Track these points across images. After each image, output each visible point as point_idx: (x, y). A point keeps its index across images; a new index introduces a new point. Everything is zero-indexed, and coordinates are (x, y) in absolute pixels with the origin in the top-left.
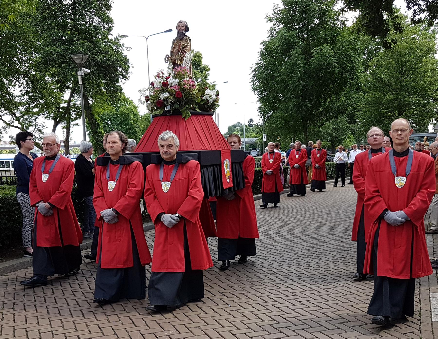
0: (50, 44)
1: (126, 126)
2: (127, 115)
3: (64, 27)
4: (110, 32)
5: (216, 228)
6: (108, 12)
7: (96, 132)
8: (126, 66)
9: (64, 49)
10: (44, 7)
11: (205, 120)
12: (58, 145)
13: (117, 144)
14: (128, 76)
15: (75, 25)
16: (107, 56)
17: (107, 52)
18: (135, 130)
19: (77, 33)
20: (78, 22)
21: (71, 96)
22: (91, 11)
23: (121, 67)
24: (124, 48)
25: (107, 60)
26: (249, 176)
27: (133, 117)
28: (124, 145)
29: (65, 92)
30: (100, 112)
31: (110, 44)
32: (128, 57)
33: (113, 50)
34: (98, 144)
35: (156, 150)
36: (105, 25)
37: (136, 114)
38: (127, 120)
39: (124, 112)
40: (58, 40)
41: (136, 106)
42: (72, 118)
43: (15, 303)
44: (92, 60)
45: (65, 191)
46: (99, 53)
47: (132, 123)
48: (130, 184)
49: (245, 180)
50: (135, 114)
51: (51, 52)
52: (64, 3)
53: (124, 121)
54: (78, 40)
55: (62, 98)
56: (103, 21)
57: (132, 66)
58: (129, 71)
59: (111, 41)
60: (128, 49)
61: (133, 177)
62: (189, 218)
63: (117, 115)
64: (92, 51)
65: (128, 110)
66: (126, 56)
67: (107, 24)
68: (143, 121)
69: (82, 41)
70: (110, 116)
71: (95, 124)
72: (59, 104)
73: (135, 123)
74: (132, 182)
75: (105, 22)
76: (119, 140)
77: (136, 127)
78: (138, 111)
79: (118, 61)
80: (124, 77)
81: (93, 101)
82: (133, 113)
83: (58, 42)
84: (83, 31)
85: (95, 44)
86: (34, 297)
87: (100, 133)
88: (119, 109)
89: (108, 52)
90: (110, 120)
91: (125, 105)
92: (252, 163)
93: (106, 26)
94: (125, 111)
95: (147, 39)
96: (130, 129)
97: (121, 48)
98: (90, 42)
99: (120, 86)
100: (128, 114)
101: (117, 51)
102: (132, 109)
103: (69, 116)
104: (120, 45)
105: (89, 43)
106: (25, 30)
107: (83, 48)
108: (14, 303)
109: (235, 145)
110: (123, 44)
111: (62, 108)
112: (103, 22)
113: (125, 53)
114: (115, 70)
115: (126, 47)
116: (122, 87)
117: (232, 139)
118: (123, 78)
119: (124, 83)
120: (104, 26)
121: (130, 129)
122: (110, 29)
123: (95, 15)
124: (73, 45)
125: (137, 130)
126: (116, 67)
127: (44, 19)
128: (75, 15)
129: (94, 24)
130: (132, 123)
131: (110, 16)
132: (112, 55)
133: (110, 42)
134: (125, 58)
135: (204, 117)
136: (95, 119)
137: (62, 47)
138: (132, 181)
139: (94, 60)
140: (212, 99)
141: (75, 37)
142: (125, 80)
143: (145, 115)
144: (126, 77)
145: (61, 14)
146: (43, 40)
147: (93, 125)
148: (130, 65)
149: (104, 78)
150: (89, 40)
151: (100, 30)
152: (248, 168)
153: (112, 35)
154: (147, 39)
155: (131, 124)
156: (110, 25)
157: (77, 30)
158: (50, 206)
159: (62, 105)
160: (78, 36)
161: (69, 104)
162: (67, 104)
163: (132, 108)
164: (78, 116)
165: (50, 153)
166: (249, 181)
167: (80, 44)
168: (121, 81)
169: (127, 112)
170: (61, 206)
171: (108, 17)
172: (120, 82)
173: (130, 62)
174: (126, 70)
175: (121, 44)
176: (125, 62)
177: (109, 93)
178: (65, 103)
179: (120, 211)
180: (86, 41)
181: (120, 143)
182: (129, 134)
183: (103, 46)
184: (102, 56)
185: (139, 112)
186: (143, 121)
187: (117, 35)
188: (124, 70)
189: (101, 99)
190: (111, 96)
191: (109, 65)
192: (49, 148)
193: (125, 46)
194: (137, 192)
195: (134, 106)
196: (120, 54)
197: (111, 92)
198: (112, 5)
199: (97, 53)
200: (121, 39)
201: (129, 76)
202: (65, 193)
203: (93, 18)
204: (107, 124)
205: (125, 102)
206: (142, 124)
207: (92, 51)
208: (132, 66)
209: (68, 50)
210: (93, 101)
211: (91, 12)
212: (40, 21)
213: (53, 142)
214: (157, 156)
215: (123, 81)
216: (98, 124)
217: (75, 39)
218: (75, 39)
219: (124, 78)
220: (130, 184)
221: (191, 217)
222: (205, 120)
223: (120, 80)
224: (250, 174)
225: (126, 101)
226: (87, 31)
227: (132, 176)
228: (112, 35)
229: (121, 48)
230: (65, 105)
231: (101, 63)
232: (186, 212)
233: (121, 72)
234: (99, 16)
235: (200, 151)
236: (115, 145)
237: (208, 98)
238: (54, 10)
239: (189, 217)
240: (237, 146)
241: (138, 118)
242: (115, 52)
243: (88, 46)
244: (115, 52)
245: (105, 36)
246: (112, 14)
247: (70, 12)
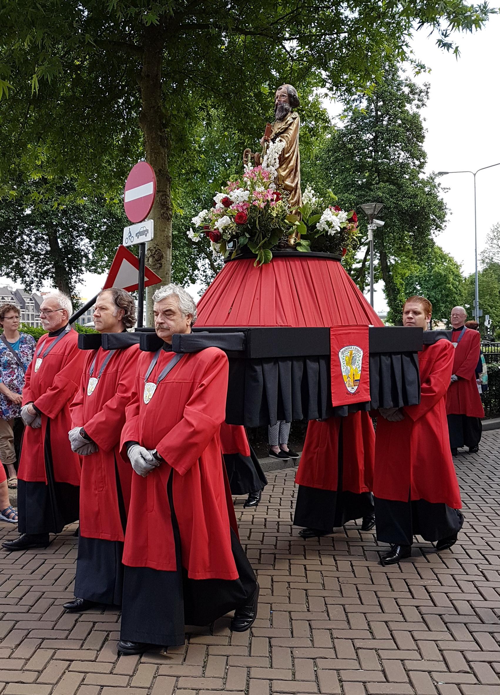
0: (342, 191)
1: (441, 291)
2: (445, 276)
3: (361, 168)
4: (422, 170)
5: (373, 468)
6: (420, 144)
7: (395, 299)
8: (441, 212)
9: (359, 196)
10: (337, 146)
11: (307, 270)
12: (65, 312)
13: (106, 312)
14: (443, 226)
15: (375, 164)
16: (416, 201)
17: (415, 196)
18: (455, 297)
19: (376, 174)
20: (379, 161)
21: (367, 253)
22: (398, 144)
23: (434, 213)
24: (439, 189)
25: (415, 206)
26: (434, 378)
27: (453, 279)
28: (123, 312)
29: (360, 249)
30: (405, 274)
31: (421, 185)
32: (444, 201)
33: (424, 192)
34: (396, 316)
35: (237, 324)
36: (415, 161)
37: (457, 276)
38: (443, 283)
39: (440, 274)
40: (353, 184)
41: (459, 264)
42: (367, 281)
43: (244, 513)
44: (394, 208)
45: (58, 388)
46: (405, 197)
47: (450, 287)
48: (118, 384)
49: (425, 385)
50: (456, 276)
51: (343, 200)
52: (364, 138)
53: (439, 285)
54: (377, 184)
55: (355, 257)
56: (412, 156)
57: (450, 211)
58: (445, 219)
59: (423, 181)
60: (446, 190)
61: (125, 372)
62: (173, 463)
63: (430, 276)
64: (395, 195)
65: (445, 270)
66: (442, 199)
67: (418, 159)
68: (467, 285)
69: (382, 184)
70: (420, 278)
71: (394, 290)
72: (350, 265)
73: (455, 288)
74: (121, 382)
75: (415, 157)
76: (112, 303)
77: (457, 294)
78: (461, 271)
79: (430, 207)
80: (438, 227)
81: (395, 260)
82: (453, 274)
83: (352, 187)
84: (385, 171)
85: (400, 186)
86: (268, 509)
87: (401, 302)
88: (433, 268)
89: (417, 195)
90: (420, 284)
91: (443, 264)
92: (446, 354)
93: (417, 163)
94: (441, 271)
95: (475, 175)
96: (447, 296)
97: (435, 190)
98: (394, 185)
99: (432, 240)
100: (445, 276)
101: (429, 194)
102: (451, 269)
103: (362, 280)
104: (435, 185)
105: (392, 187)
106: (312, 177)
107: (383, 193)
108: (242, 512)
109: (417, 317)
110: (439, 184)
111: (355, 270)
112: (413, 158)
113: (441, 195)
114: (425, 219)
115: (443, 187)
116: (435, 240)
117: (411, 305)
118: (436, 229)
119: (437, 234)
120: (414, 163)
121: (447, 296)
122: (421, 166)
123: (402, 150)
124: (371, 190)
125: (457, 298)
126: (428, 214)
127: (337, 160)
128: (376, 151)
129: (401, 161)
130: (450, 287)
131: (423, 149)
132: (422, 200)
133: (421, 182)
134: (441, 203)
135: (304, 263)
136: (394, 284)
137: (357, 193)
138: (121, 381)
139: (396, 208)
140: (333, 229)
141: (374, 179)
142: (439, 231)
143: (471, 276)
144: (440, 227)
145: (358, 152)
146: (334, 186)
147: (391, 291)
148: (447, 211)
149: (410, 229)
150: (392, 183)
151: (408, 168)
152: (435, 362)
153: (424, 173)
154: (475, 175)
155: (449, 289)
156: (422, 160)
157: (378, 171)
158: (34, 411)
159: (354, 266)
160: (377, 178)
161: (364, 265)
162: (361, 264)
163: (452, 267)
164: (376, 279)
165: (48, 324)
166: (431, 388)
167: (380, 188)
168: (434, 233)
169: (443, 273)
170: (50, 412)
171: (420, 150)
172: (432, 234)
173: (447, 207)
174: (441, 218)
175: (437, 184)
176: (441, 206)
177: (416, 249)
178: (358, 263)
179: (92, 434)
180: (387, 184)
181: (113, 309)
182: (446, 302)
183: (410, 189)
184: (409, 201)
185: (462, 273)
186: (467, 285)
187: (431, 172)
188: (439, 218)
189: (407, 257)
190: (418, 252)
191: (418, 212)
192: (47, 317)
193: (441, 186)
194: (124, 400)
195: (455, 265)
196: (434, 197)
197: (418, 247)
198: (425, 135)
199: (402, 198)
200: (437, 177)
201: (445, 226)
202: (465, 368)
203: (399, 154)
204: (415, 288)
205: (442, 259)
206: (465, 290)
207: (395, 195)
208: (450, 211)
209: (364, 196)
210: (395, 260)
211: (396, 147)
212: (331, 164)
213: (54, 306)
214: (148, 336)
215: (437, 232)
216: (398, 289)
217: (374, 183)
218: (374, 183)
219: (438, 229)
220: (118, 384)
221: (175, 460)
222: (307, 270)
223: (432, 231)
224: (436, 373)
225: (444, 257)
226: (390, 172)
227: (123, 370)
228: (424, 173)
229: (435, 190)
230: (359, 266)
231: (407, 211)
232: (169, 449)
233: (434, 220)
234: (408, 151)
235: (249, 329)
236: (102, 313)
237: (327, 227)
238: (350, 149)
239: (172, 460)
240: (420, 319)
241: (460, 281)
242: (427, 195)
243: (391, 191)
244: (427, 195)
245: (414, 176)
246: (426, 146)
247: (371, 148)
